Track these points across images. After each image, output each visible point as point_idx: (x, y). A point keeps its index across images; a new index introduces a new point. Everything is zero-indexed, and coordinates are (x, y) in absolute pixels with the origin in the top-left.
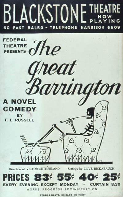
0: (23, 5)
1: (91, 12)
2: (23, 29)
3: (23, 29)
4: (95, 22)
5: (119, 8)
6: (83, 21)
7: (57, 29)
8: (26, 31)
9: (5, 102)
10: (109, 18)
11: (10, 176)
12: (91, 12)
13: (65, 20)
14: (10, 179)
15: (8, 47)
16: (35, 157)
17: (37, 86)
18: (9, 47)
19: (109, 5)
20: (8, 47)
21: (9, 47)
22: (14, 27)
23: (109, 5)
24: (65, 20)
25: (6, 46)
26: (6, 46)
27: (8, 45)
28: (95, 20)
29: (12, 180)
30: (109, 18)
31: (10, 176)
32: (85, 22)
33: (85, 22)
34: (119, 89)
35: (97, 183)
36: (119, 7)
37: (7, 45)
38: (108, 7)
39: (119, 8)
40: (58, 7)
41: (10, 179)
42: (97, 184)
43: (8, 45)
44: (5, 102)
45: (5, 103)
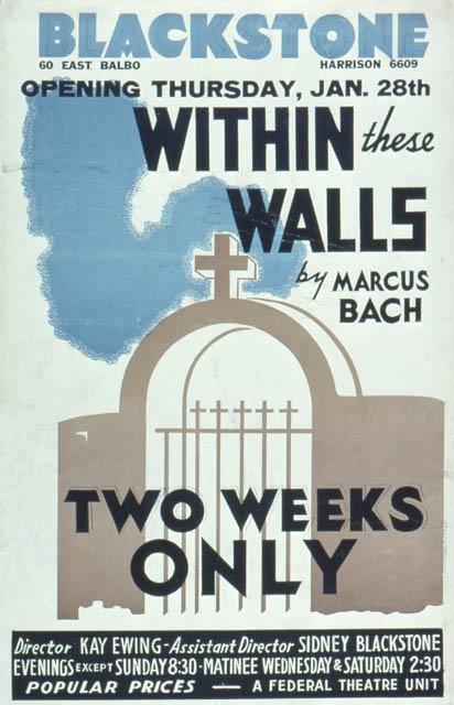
0: (211, 23)
4: (212, 297)
8: (168, 637)
9: (269, 89)
11: (376, 278)
14: (271, 149)
15: (178, 93)
16: (243, 610)
18: (184, 94)
20: (178, 93)
21: (184, 94)
22: (83, 644)
25: (166, 89)
27: (178, 84)
29: (282, 164)
31: (376, 278)
34: (227, 507)
35: (210, 83)
37: (172, 83)
38: (223, 663)
41: (271, 149)
42: (210, 89)
43: (178, 84)
44: (335, 89)
45: (269, 93)
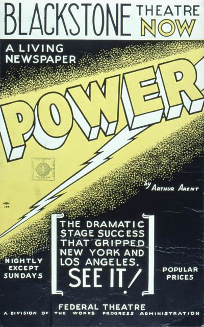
1: (112, 285)
2: (86, 245)
3: (86, 245)
5: (99, 276)
6: (22, 50)
7: (62, 264)
10: (24, 61)
12: (112, 285)
13: (37, 61)
17: (11, 15)
19: (125, 222)
23: (125, 222)
24: (37, 61)
26: (143, 9)
27: (149, 8)
28: (20, 46)
30: (26, 61)
31: (10, 8)
32: (24, 51)
33: (24, 51)
36: (98, 273)
39: (99, 276)
40: (65, 242)
43: (149, 8)
